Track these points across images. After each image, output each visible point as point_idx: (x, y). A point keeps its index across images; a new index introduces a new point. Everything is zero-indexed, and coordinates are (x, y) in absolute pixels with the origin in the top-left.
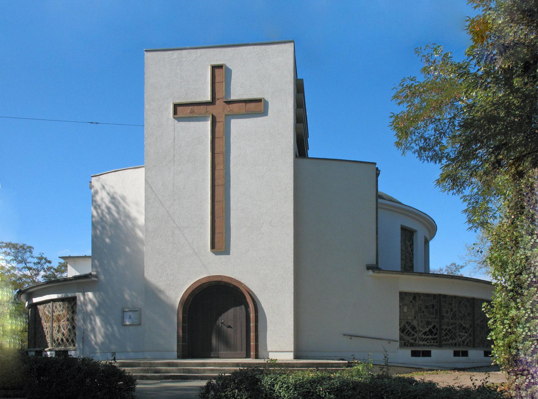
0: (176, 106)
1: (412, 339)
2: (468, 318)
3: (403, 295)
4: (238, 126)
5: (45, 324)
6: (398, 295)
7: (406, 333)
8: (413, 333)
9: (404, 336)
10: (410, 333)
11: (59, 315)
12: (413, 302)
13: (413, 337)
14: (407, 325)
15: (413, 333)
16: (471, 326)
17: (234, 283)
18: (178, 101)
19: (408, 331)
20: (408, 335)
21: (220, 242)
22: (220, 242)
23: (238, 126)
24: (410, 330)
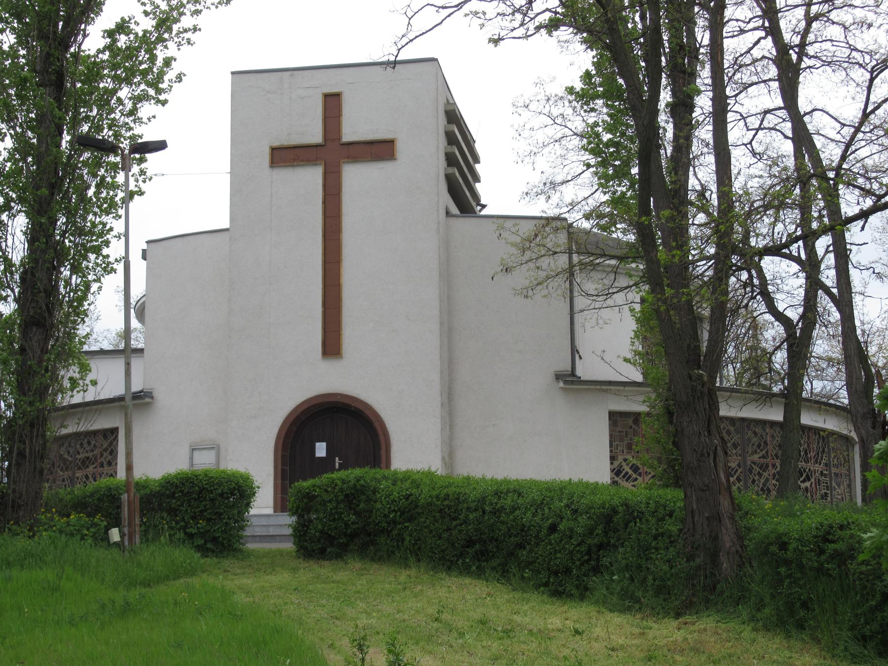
0: (273, 150)
1: (634, 486)
2: (734, 451)
3: (612, 415)
4: (315, 135)
5: (61, 473)
6: (141, 252)
7: (624, 477)
8: (634, 476)
9: (620, 481)
10: (630, 477)
11: (87, 458)
12: (634, 426)
13: (635, 483)
14: (624, 464)
15: (634, 476)
16: (739, 465)
17: (326, 400)
18: (276, 144)
19: (627, 473)
20: (627, 480)
21: (332, 346)
22: (332, 346)
23: (315, 135)
24: (630, 472)
